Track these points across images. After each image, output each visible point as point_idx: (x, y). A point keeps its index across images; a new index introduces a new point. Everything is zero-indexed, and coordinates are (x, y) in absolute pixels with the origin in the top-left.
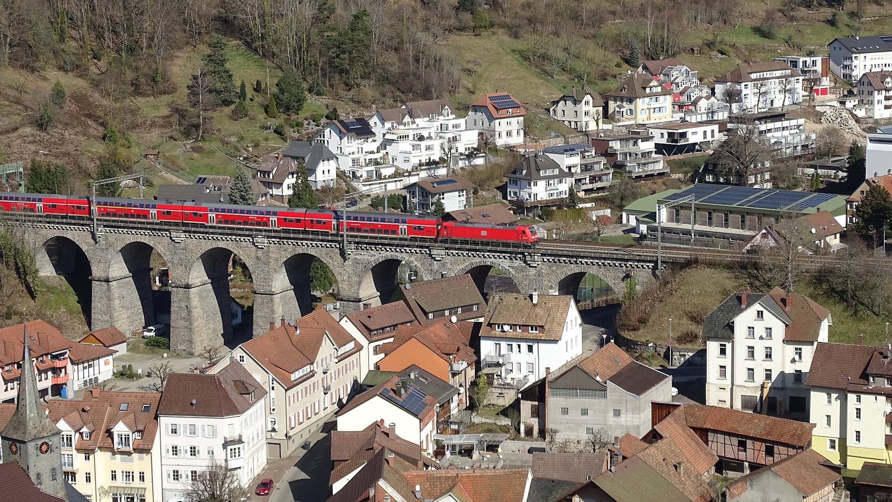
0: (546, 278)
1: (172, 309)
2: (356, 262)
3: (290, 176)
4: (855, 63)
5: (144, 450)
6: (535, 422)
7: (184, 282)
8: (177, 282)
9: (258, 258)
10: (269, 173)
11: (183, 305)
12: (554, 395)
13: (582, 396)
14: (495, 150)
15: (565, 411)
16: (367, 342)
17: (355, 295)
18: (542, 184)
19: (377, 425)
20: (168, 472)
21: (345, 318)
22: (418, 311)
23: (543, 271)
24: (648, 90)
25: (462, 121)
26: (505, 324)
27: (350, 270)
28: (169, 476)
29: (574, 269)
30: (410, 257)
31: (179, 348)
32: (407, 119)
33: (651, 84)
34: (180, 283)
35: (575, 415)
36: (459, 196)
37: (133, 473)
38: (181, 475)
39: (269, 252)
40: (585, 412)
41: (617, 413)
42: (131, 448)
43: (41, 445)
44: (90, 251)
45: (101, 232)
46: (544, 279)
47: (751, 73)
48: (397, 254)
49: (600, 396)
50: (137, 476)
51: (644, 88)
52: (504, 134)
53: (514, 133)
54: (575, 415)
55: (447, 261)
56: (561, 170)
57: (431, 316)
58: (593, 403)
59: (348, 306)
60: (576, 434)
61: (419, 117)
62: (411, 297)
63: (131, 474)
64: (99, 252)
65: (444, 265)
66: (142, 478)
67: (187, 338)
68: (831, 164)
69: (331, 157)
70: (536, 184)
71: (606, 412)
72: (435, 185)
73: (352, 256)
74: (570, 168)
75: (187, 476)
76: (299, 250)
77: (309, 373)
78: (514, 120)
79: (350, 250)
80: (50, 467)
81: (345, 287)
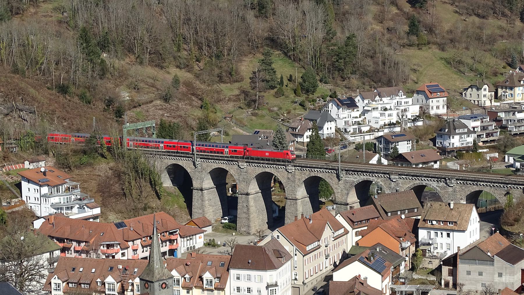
0: (459, 194)
1: (238, 207)
2: (346, 182)
3: (308, 131)
6: (450, 279)
7: (245, 192)
9: (288, 178)
12: (462, 263)
13: (479, 264)
14: (429, 117)
15: (469, 273)
17: (345, 201)
18: (457, 137)
22: (382, 212)
23: (457, 189)
26: (433, 220)
27: (342, 186)
29: (476, 188)
31: (242, 230)
32: (377, 98)
35: (474, 275)
36: (408, 144)
40: (480, 274)
41: (500, 275)
43: (162, 284)
44: (192, 173)
45: (198, 161)
49: (490, 265)
52: (435, 108)
54: (474, 275)
55: (400, 182)
56: (469, 129)
57: (389, 214)
58: (485, 268)
59: (341, 208)
61: (384, 97)
62: (378, 203)
64: (197, 173)
65: (398, 184)
67: (247, 224)
69: (332, 120)
70: (453, 138)
71: (493, 274)
72: (393, 137)
73: (344, 178)
74: (474, 128)
76: (313, 174)
77: (317, 246)
78: (441, 99)
79: (343, 174)
81: (339, 196)
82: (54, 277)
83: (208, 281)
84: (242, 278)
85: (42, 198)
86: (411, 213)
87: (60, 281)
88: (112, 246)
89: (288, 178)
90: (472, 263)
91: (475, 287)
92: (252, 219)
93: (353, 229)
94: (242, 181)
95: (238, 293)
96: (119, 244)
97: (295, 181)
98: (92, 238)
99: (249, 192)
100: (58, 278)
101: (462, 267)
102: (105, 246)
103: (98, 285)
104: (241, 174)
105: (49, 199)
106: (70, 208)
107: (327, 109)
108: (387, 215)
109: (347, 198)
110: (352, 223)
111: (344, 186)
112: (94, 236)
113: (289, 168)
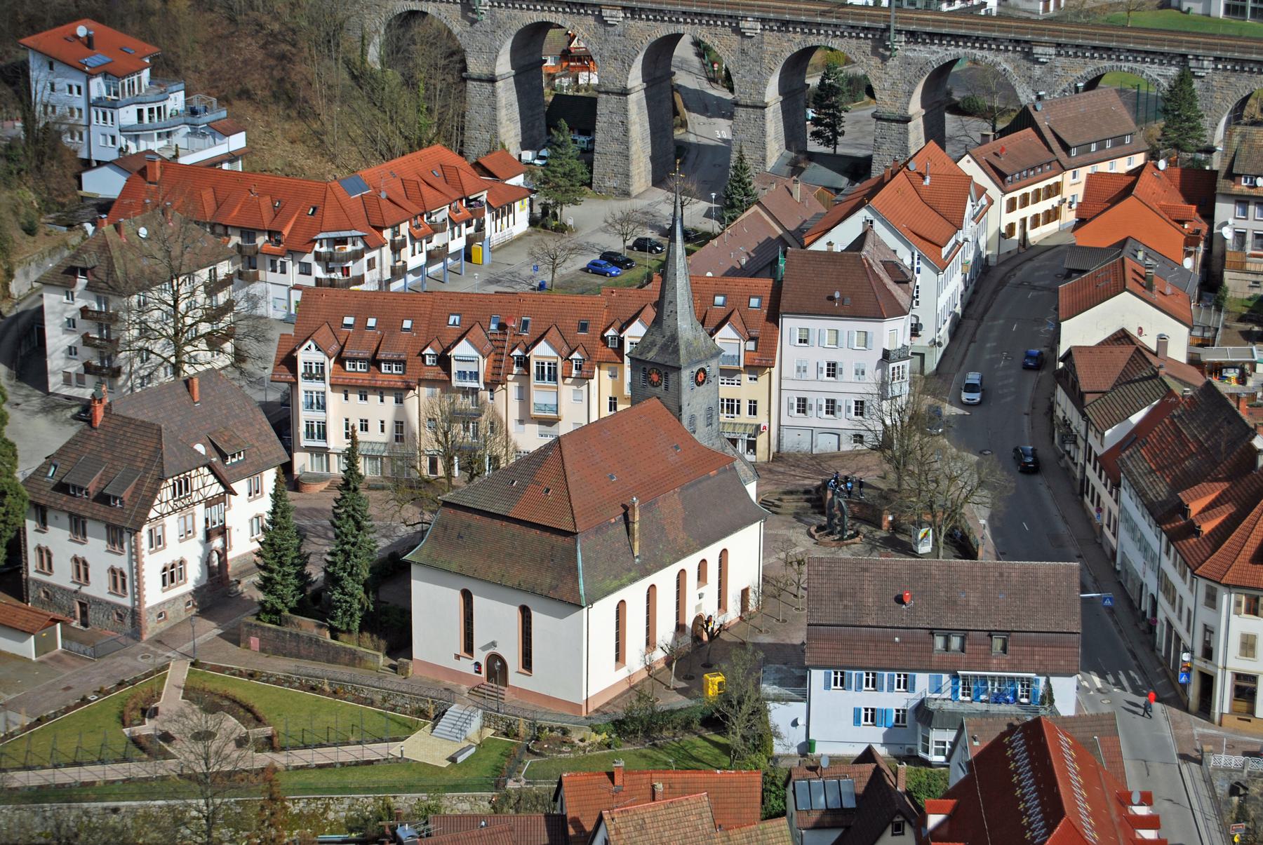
0: (1218, 95)
1: (599, 125)
2: (907, 62)
5: (756, 368)
7: (618, 85)
8: (607, 84)
9: (743, 51)
11: (617, 119)
16: (1000, 193)
20: (791, 401)
21: (967, 157)
22: (1055, 145)
23: (1214, 83)
26: (1257, 176)
27: (895, 73)
28: (791, 406)
30: (996, 56)
31: (608, 184)
34: (612, 86)
37: (738, 401)
38: (811, 405)
39: (762, 43)
42: (742, 366)
43: (698, 373)
44: (465, 34)
46: (1215, 95)
48: (974, 51)
50: (745, 407)
55: (1058, 64)
57: (1074, 152)
62: (1043, 125)
63: (736, 403)
64: (480, 37)
65: (1051, 70)
66: (753, 410)
67: (621, 170)
73: (900, 53)
80: (705, 406)
81: (887, 99)
82: (306, 346)
83: (543, 368)
84: (813, 338)
85: (93, 109)
86: (1119, 148)
88: (343, 241)
89: (743, 51)
92: (635, 157)
93: (1005, 193)
94: (610, 57)
96: (362, 237)
97: (762, 58)
98: (286, 222)
102: (325, 242)
103: (428, 363)
104: (606, 40)
105: (115, 112)
106: (165, 136)
109: (908, 104)
110: (1000, 177)
111: (901, 74)
113: (747, 25)
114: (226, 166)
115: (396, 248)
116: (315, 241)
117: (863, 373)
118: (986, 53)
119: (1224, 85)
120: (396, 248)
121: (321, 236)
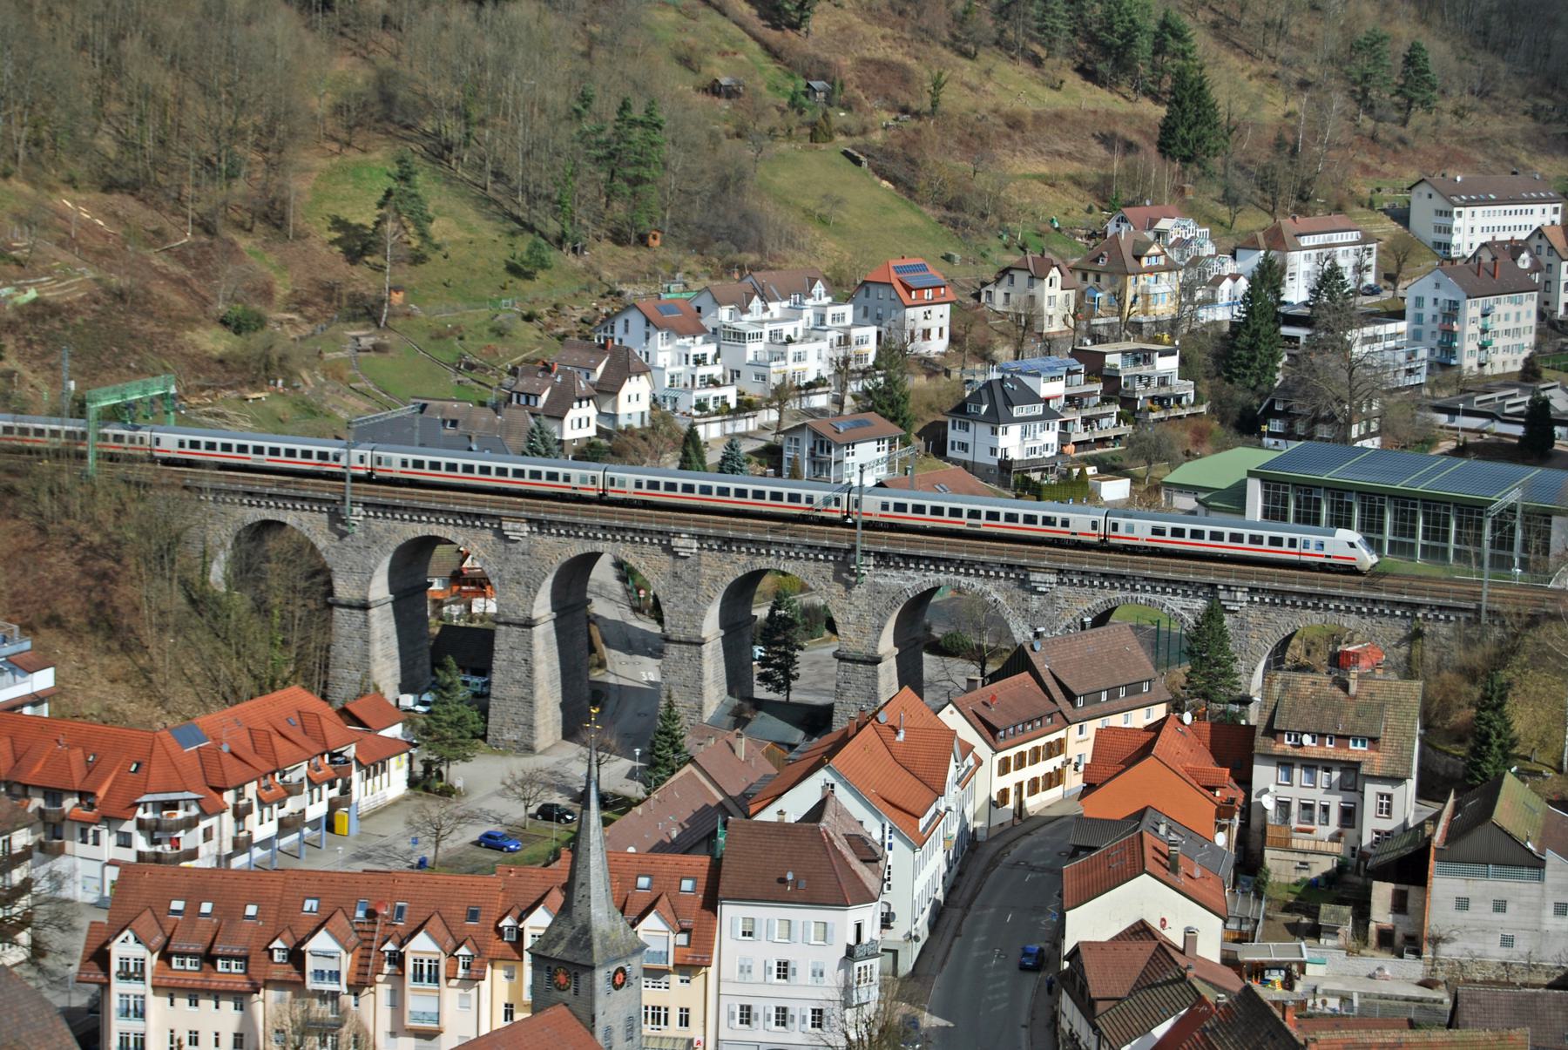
0: (1255, 633)
1: (496, 664)
2: (877, 590)
3: (576, 405)
4: (1457, 223)
9: (675, 575)
10: (537, 396)
11: (519, 657)
12: (1442, 873)
13: (1497, 876)
15: (1463, 904)
17: (870, 651)
18: (1015, 430)
19: (1141, 930)
22: (1057, 693)
24: (1144, 262)
25: (848, 310)
27: (862, 604)
31: (507, 736)
32: (756, 303)
33: (1151, 251)
34: (513, 616)
35: (1481, 912)
40: (1500, 906)
47: (1301, 235)
49: (1531, 878)
50: (674, 1017)
51: (1138, 258)
53: (934, 334)
54: (1481, 912)
57: (1080, 702)
59: (854, 671)
60: (1482, 946)
61: (775, 299)
62: (1043, 668)
63: (663, 1012)
64: (350, 553)
65: (1052, 601)
66: (685, 1021)
68: (1476, 407)
69: (644, 370)
71: (1541, 907)
73: (868, 579)
75: (804, 1018)
79: (867, 566)
80: (625, 1016)
81: (852, 636)
86: (1134, 698)
87: (140, 951)
88: (173, 805)
89: (675, 575)
90: (1474, 875)
91: (1482, 946)
94: (512, 580)
95: (782, 981)
96: (197, 800)
99: (534, 616)
100: (138, 941)
101: (1444, 886)
102: (150, 806)
103: (276, 959)
107: (609, 334)
108: (1074, 705)
110: (990, 731)
112: (110, 772)
114: (27, 711)
115: (240, 814)
116: (138, 805)
117: (822, 974)
118: (972, 580)
119: (1262, 622)
120: (240, 814)
121: (145, 798)
